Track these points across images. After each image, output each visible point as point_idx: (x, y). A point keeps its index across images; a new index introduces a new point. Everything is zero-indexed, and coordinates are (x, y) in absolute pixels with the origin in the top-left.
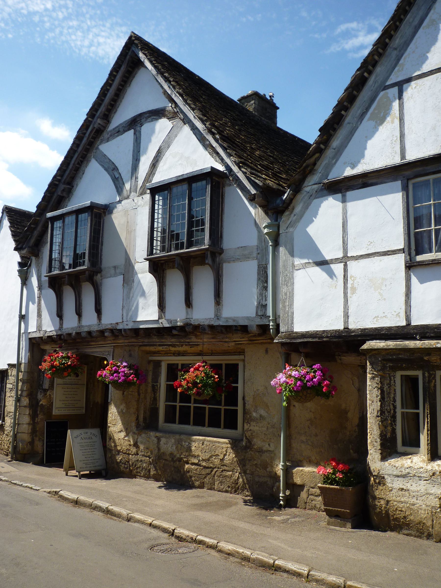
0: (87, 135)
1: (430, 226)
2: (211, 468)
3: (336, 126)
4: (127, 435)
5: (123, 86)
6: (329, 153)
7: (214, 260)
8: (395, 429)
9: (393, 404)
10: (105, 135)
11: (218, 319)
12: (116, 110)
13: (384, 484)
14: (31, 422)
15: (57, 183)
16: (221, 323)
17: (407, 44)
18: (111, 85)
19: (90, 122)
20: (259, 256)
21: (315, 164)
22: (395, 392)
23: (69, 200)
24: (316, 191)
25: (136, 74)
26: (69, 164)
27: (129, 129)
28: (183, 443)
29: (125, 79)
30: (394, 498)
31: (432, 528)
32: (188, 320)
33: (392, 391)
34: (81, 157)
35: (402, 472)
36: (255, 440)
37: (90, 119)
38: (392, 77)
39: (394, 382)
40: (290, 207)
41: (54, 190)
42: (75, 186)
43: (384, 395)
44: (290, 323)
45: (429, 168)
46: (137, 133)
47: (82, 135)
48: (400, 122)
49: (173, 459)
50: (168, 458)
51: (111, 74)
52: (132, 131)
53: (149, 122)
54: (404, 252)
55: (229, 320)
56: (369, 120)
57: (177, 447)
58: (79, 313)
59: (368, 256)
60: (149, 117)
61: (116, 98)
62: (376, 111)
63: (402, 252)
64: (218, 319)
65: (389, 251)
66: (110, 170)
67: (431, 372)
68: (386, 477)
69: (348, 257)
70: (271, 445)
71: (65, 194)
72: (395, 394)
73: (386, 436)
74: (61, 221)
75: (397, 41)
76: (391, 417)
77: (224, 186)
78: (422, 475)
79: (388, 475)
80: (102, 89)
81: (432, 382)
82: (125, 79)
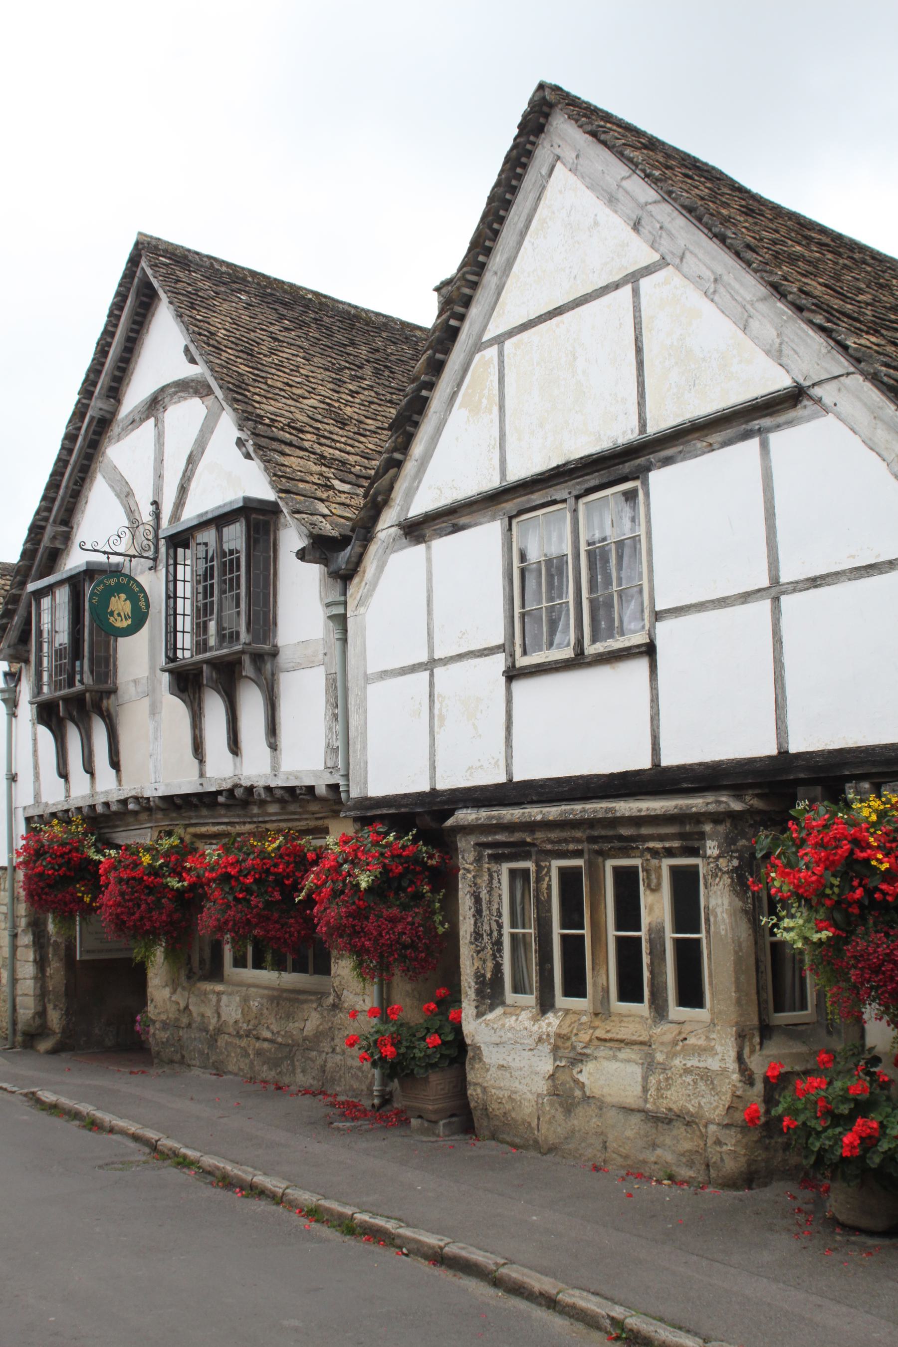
0: (83, 431)
1: (540, 602)
2: (288, 1045)
3: (415, 417)
4: (174, 992)
5: (138, 332)
6: (410, 467)
7: (259, 670)
8: (501, 964)
9: (497, 921)
10: (116, 429)
11: (275, 775)
12: (130, 380)
13: (481, 1060)
14: (40, 975)
15: (42, 523)
16: (280, 782)
17: (509, 264)
18: (113, 335)
19: (87, 406)
20: (326, 658)
21: (391, 488)
22: (501, 899)
23: (68, 555)
24: (394, 540)
25: (156, 308)
26: (58, 487)
27: (148, 418)
28: (252, 1003)
29: (137, 318)
30: (492, 1082)
31: (538, 1130)
32: (236, 778)
33: (496, 899)
34: (80, 471)
35: (501, 1037)
36: (345, 992)
37: (85, 401)
38: (490, 326)
39: (499, 882)
40: (361, 569)
41: (39, 537)
42: (75, 527)
43: (481, 905)
44: (363, 781)
45: (534, 496)
46: (159, 425)
47: (74, 432)
48: (500, 411)
49: (238, 1032)
50: (231, 1030)
51: (111, 315)
52: (152, 421)
53: (175, 403)
54: (504, 651)
55: (290, 777)
56: (460, 407)
57: (242, 1012)
58: (234, 746)
59: (460, 657)
60: (175, 393)
61: (127, 355)
62: (470, 391)
63: (501, 650)
64: (275, 775)
65: (485, 649)
66: (123, 496)
67: (543, 864)
68: (483, 1047)
69: (435, 660)
70: (366, 1001)
71: (58, 545)
72: (500, 903)
73: (484, 976)
74: (50, 597)
75: (497, 260)
76: (493, 944)
77: (276, 529)
78: (525, 1042)
79: (485, 1043)
80: (98, 344)
81: (544, 880)
82: (137, 318)
